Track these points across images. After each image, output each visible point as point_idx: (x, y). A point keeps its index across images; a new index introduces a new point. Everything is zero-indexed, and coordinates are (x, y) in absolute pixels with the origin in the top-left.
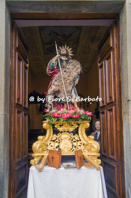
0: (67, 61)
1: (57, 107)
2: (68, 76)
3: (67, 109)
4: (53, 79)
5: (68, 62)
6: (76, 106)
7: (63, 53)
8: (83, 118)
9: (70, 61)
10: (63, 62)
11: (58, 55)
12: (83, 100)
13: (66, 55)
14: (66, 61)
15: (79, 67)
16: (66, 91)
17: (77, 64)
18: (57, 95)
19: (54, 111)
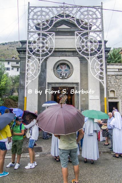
12: (77, 93)
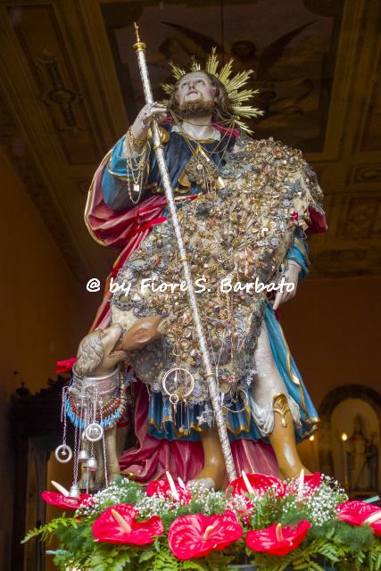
0: (218, 151)
1: (149, 463)
2: (224, 245)
3: (221, 483)
4: (120, 265)
5: (227, 155)
6: (288, 455)
7: (193, 97)
8: (331, 553)
9: (236, 149)
10: (190, 155)
11: (151, 108)
13: (217, 112)
14: (209, 146)
15: (298, 183)
16: (212, 346)
17: (282, 167)
18: (145, 377)
19: (109, 496)
